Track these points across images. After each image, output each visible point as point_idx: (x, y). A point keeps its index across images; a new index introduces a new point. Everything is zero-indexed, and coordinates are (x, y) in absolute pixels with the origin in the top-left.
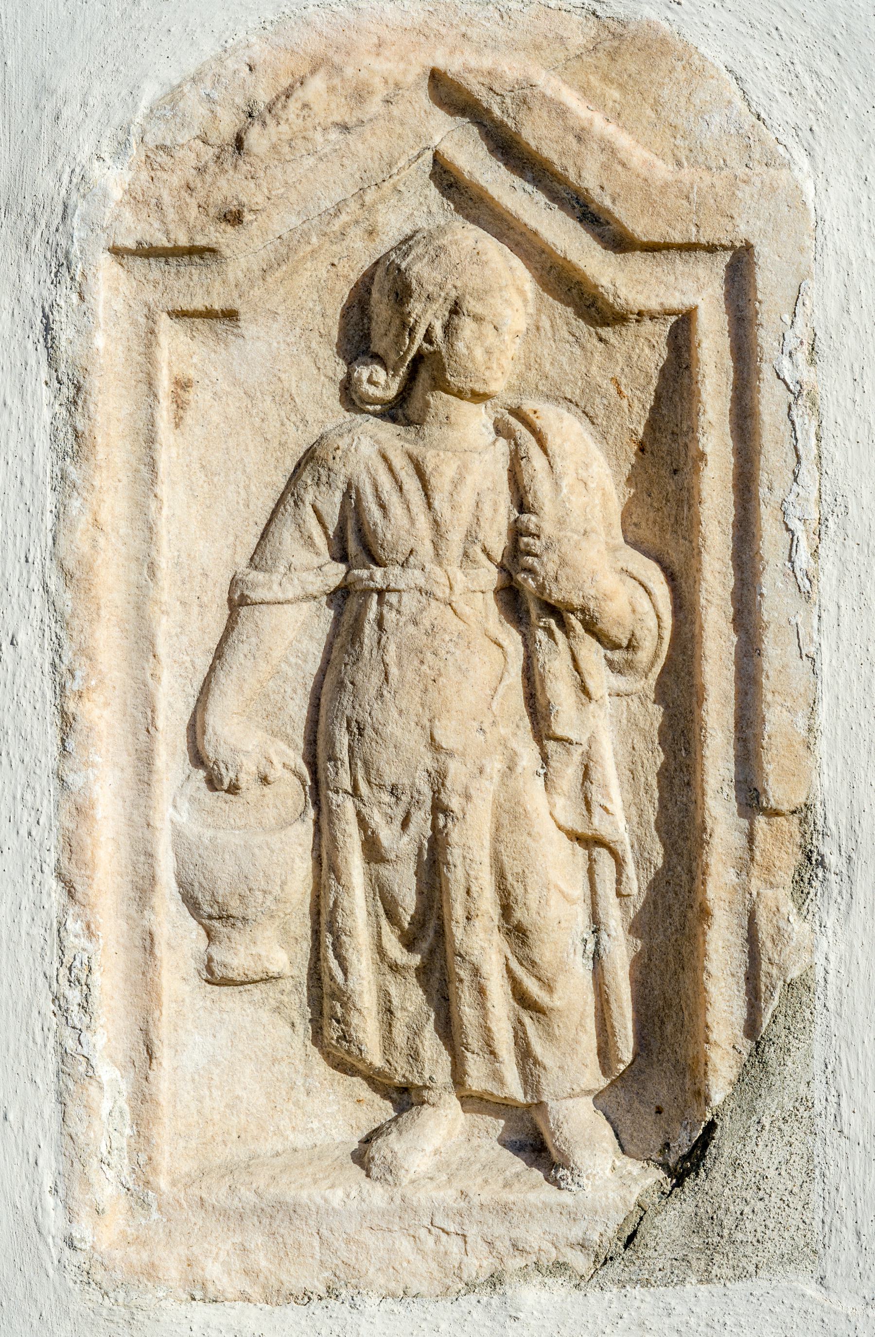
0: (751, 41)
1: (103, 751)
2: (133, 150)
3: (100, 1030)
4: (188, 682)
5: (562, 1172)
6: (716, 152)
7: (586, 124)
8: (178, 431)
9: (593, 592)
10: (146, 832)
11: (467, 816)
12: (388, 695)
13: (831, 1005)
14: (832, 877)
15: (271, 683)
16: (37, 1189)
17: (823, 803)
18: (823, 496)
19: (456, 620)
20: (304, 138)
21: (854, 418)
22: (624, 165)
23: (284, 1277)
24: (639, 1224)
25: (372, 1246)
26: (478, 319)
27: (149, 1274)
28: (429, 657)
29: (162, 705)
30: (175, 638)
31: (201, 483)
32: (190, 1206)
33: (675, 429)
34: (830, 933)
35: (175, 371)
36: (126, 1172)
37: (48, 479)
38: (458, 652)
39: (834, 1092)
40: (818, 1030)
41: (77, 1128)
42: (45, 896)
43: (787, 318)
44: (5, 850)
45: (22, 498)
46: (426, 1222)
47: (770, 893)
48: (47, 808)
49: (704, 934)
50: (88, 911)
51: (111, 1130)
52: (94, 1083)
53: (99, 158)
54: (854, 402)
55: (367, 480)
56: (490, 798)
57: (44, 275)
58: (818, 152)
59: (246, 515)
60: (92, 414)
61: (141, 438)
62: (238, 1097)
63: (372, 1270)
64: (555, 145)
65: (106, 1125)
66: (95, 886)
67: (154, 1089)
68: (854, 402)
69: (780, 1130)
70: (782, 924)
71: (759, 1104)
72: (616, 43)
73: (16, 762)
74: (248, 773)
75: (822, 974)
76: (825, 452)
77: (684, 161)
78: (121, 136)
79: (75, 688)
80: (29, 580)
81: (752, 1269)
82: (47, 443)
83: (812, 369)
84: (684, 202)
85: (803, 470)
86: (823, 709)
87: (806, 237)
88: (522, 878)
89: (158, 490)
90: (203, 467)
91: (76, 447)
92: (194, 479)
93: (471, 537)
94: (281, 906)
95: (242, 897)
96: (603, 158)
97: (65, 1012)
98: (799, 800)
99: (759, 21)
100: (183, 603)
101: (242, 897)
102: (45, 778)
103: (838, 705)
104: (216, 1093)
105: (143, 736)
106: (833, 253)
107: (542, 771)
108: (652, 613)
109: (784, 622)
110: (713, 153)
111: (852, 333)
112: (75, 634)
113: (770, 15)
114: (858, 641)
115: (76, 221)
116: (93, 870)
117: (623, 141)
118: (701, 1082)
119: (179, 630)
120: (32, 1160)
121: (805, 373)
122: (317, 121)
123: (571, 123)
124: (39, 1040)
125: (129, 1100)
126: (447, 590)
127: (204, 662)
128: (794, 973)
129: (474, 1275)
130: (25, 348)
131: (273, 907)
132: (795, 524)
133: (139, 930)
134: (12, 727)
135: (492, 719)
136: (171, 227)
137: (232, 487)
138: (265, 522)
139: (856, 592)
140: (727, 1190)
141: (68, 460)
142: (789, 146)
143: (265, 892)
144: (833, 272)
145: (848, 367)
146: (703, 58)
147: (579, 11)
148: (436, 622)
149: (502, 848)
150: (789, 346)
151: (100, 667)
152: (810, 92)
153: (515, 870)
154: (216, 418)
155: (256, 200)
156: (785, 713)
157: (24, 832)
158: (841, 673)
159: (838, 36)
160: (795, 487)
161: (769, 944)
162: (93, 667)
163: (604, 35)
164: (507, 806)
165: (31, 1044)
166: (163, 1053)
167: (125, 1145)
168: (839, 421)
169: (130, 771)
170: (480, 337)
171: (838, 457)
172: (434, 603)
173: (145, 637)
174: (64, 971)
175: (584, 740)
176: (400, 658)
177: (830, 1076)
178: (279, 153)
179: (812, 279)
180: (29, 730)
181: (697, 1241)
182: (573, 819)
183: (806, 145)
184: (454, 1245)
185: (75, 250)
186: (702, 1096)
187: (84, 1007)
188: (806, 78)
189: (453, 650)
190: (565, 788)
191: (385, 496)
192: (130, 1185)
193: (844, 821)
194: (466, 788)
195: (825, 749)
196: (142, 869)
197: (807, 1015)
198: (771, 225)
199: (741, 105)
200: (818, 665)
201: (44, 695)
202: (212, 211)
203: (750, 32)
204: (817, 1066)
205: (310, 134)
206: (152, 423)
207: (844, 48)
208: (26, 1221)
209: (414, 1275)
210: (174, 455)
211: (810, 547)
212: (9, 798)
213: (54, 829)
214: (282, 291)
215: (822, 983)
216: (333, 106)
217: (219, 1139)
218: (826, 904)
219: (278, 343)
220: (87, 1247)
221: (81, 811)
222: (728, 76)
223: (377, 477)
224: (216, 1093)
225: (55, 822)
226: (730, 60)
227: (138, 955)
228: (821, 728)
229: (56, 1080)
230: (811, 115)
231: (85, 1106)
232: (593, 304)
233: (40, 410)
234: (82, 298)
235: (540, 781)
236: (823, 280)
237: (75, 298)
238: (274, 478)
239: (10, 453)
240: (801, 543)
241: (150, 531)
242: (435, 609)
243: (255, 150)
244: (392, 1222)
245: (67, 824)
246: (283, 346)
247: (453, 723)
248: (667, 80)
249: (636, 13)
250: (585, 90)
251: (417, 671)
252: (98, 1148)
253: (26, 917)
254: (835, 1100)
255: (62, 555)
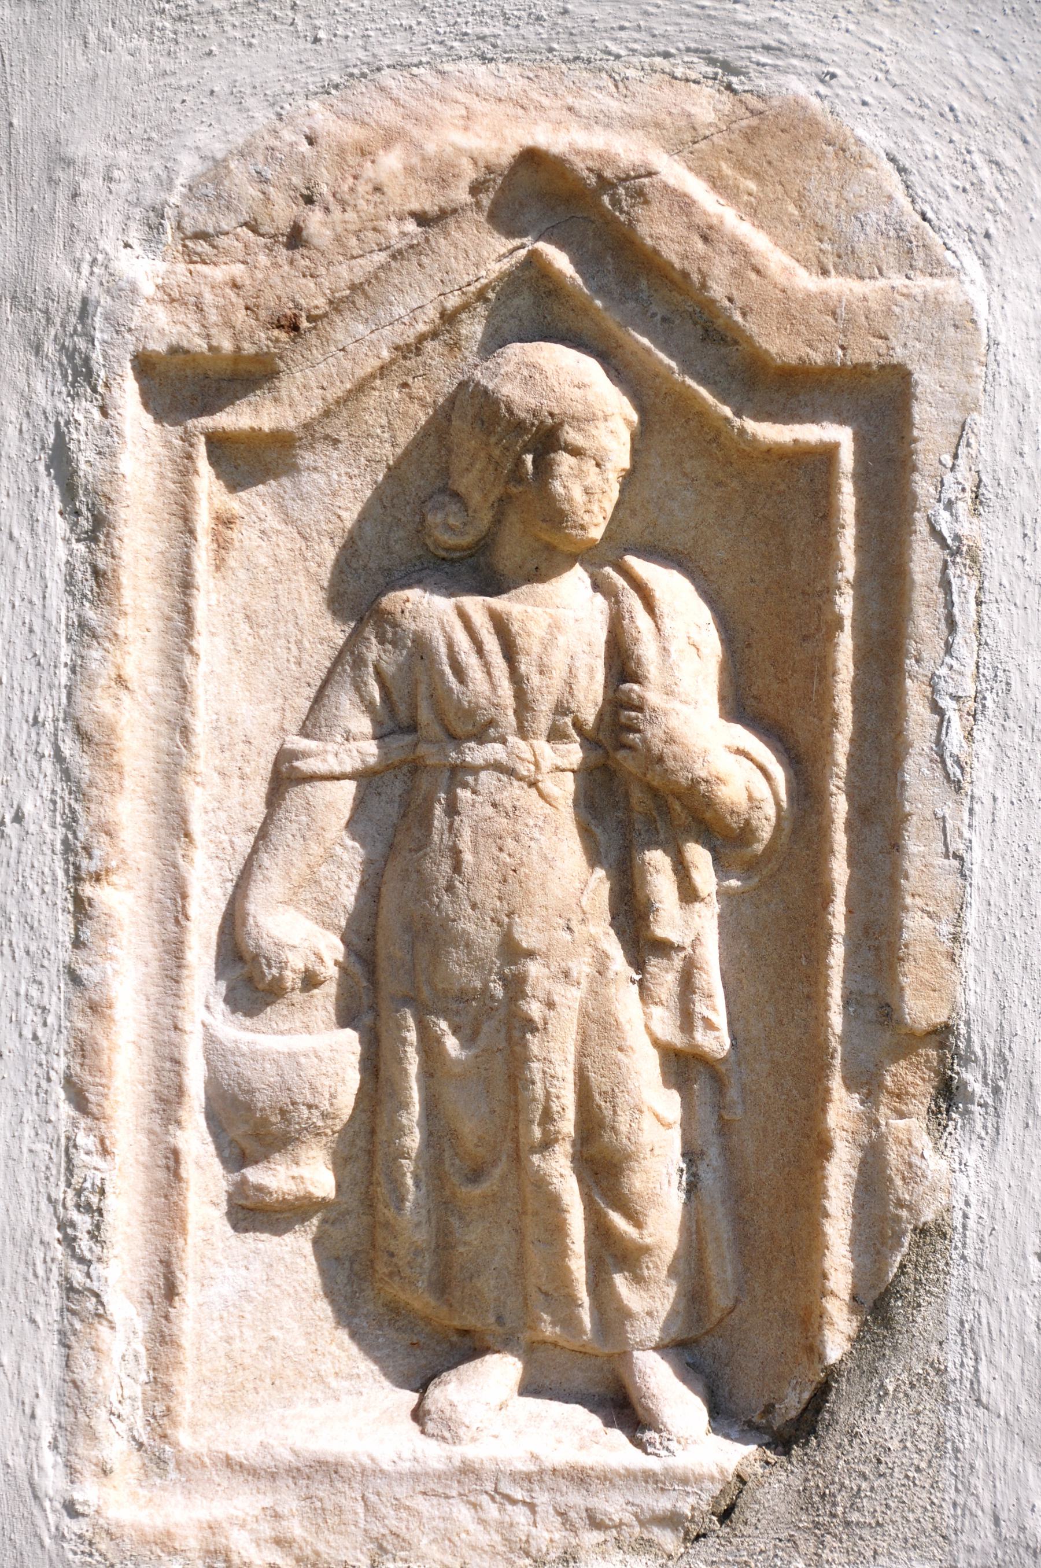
0: (920, 123)
1: (125, 942)
2: (169, 237)
3: (113, 1262)
4: (226, 864)
5: (649, 1435)
6: (871, 260)
7: (715, 221)
8: (218, 575)
9: (703, 774)
10: (172, 1034)
11: (549, 1026)
12: (460, 886)
13: (969, 1253)
14: (976, 1109)
15: (322, 869)
16: (33, 1444)
17: (968, 1023)
18: (981, 670)
19: (542, 803)
20: (375, 229)
21: (1023, 579)
22: (758, 272)
23: (322, 1547)
24: (738, 1497)
25: (426, 1514)
26: (576, 452)
27: (163, 1543)
28: (510, 844)
29: (195, 891)
30: (211, 814)
31: (244, 636)
32: (215, 1464)
33: (807, 588)
34: (971, 1172)
35: (217, 503)
36: (140, 1424)
37: (63, 627)
38: (543, 838)
39: (971, 1354)
40: (954, 1283)
41: (84, 1374)
42: (51, 1108)
43: (947, 459)
44: (5, 1052)
45: (30, 646)
46: (489, 1487)
47: (901, 1123)
48: (55, 1005)
49: (823, 1168)
50: (103, 1126)
51: (123, 1375)
52: (105, 1323)
53: (127, 245)
54: (1024, 561)
55: (441, 638)
56: (576, 1006)
57: (59, 386)
58: (995, 262)
59: (298, 675)
60: (117, 553)
61: (175, 581)
62: (273, 1338)
63: (425, 1541)
64: (677, 247)
65: (118, 1371)
66: (111, 1097)
67: (175, 1328)
68: (1024, 561)
69: (906, 1395)
70: (916, 1160)
71: (881, 1365)
72: (754, 121)
73: (20, 953)
74: (294, 971)
75: (961, 1220)
76: (986, 618)
77: (831, 268)
78: (154, 220)
79: (92, 869)
80: (38, 743)
81: (869, 1553)
82: (62, 585)
83: (975, 520)
84: (830, 319)
85: (959, 639)
86: (972, 917)
87: (974, 363)
88: (610, 1096)
89: (194, 644)
90: (247, 617)
91: (96, 589)
92: (236, 630)
93: (561, 709)
94: (330, 1122)
95: (283, 1112)
96: (732, 262)
97: (69, 1242)
98: (940, 1016)
99: (931, 98)
100: (222, 774)
101: (283, 1112)
102: (54, 971)
103: (989, 912)
104: (248, 1333)
105: (171, 927)
106: (1007, 383)
107: (637, 977)
108: (771, 801)
109: (928, 815)
110: (867, 260)
111: (1026, 480)
112: (93, 806)
113: (943, 91)
114: (1016, 839)
115: (98, 321)
116: (110, 1077)
117: (758, 241)
118: (814, 1337)
119: (217, 805)
120: (28, 1411)
121: (966, 525)
122: (391, 209)
123: (697, 220)
124: (41, 1272)
125: (145, 1340)
126: (532, 768)
127: (245, 842)
128: (928, 1216)
129: (544, 1550)
130: (36, 470)
131: (320, 1123)
132: (945, 703)
133: (162, 1146)
134: (15, 912)
135: (581, 916)
136: (214, 331)
137: (282, 642)
138: (319, 683)
139: (1016, 782)
140: (842, 1462)
141: (87, 604)
142: (959, 252)
143: (310, 1107)
144: (1006, 405)
145: (1018, 520)
146: (859, 142)
147: (710, 82)
148: (517, 804)
149: (588, 1062)
150: (949, 494)
151: (122, 845)
152: (989, 188)
153: (604, 1089)
154: (263, 560)
155: (316, 302)
156: (927, 919)
157: (28, 1034)
158: (995, 875)
159: (1027, 117)
160: (948, 659)
161: (898, 1182)
162: (113, 845)
163: (741, 111)
164: (595, 1014)
165: (30, 1276)
166: (189, 1289)
167: (140, 1396)
168: (1005, 582)
169: (155, 965)
170: (580, 474)
171: (1002, 624)
172: (516, 783)
173: (177, 812)
174: (71, 1193)
175: (687, 943)
176: (475, 844)
177: (967, 1336)
178: (343, 246)
179: (980, 413)
180: (36, 915)
181: (805, 1520)
182: (667, 1029)
183: (980, 251)
184: (520, 1515)
185: (97, 356)
186: (814, 1350)
187: (95, 1234)
188: (985, 172)
189: (537, 835)
190: (664, 997)
191: (463, 658)
192: (144, 1439)
193: (992, 1044)
194: (549, 993)
195: (972, 962)
196: (168, 1077)
197: (941, 1265)
198: (934, 348)
199: (904, 202)
200: (967, 865)
201: (55, 879)
202: (263, 314)
203: (920, 111)
204: (952, 1325)
205: (382, 224)
206: (187, 562)
207: (1033, 133)
208: (19, 1481)
209: (474, 1548)
210: (214, 602)
211: (964, 727)
212: (11, 993)
213: (63, 1030)
214: (345, 414)
215: (960, 1229)
216: (411, 191)
217: (250, 1386)
218: (967, 1139)
219: (339, 475)
220: (90, 1511)
221: (96, 1009)
222: (889, 166)
223: (454, 636)
224: (248, 1333)
225: (65, 1023)
226: (892, 145)
227: (161, 1175)
228: (968, 937)
229: (58, 1318)
230: (988, 215)
231: (93, 1349)
232: (716, 439)
233: (54, 544)
234: (104, 411)
235: (635, 988)
236: (993, 414)
237: (97, 415)
238: (332, 633)
239: (17, 594)
240: (952, 724)
241: (183, 688)
242: (517, 790)
243: (315, 241)
244: (450, 1487)
245: (80, 1025)
246: (344, 478)
247: (536, 920)
248: (815, 169)
249: (780, 86)
250: (716, 183)
251: (496, 860)
252: (107, 1397)
253: (28, 1131)
254: (972, 1363)
255: (78, 715)
